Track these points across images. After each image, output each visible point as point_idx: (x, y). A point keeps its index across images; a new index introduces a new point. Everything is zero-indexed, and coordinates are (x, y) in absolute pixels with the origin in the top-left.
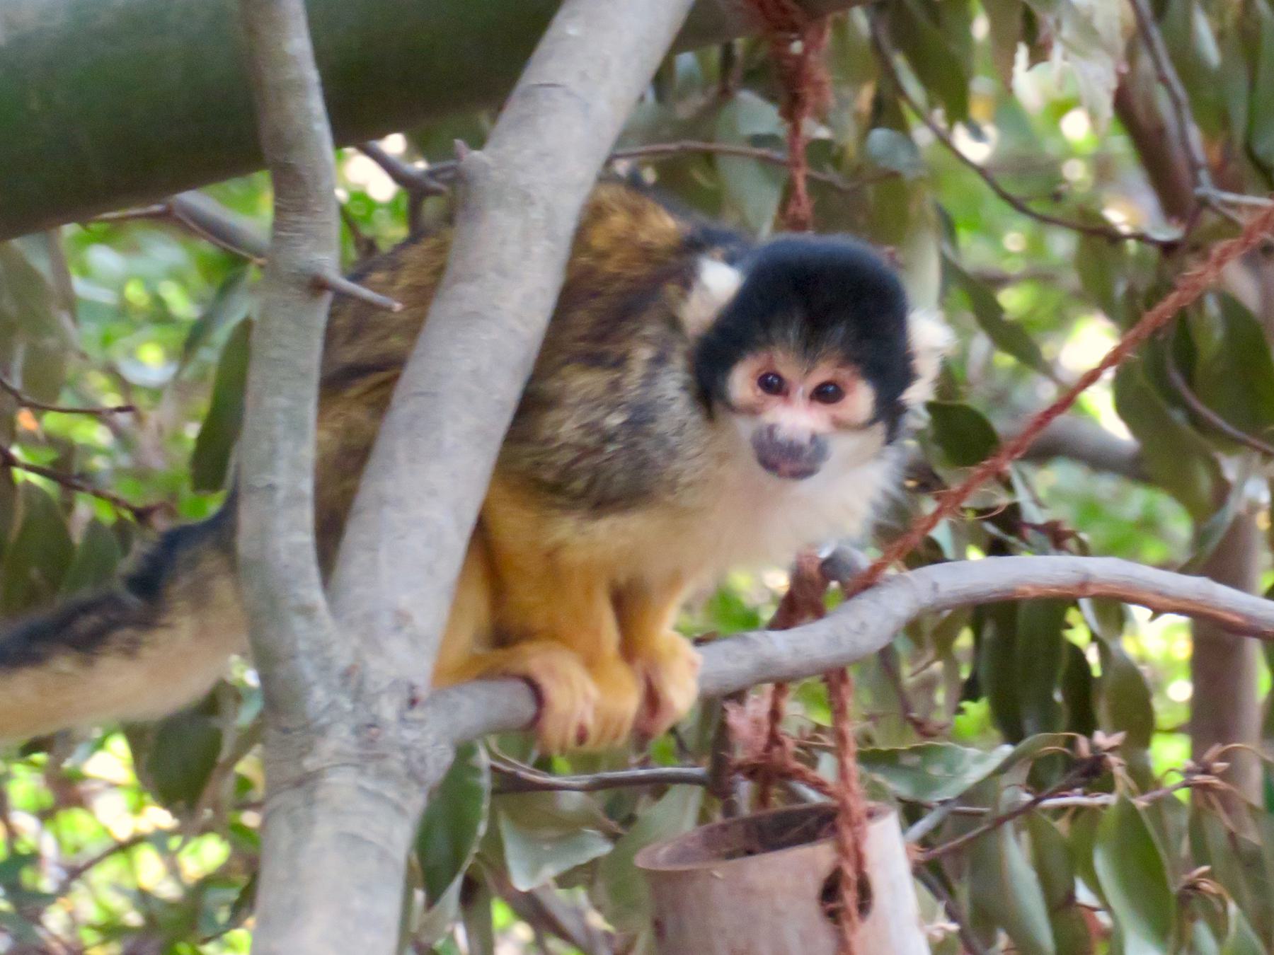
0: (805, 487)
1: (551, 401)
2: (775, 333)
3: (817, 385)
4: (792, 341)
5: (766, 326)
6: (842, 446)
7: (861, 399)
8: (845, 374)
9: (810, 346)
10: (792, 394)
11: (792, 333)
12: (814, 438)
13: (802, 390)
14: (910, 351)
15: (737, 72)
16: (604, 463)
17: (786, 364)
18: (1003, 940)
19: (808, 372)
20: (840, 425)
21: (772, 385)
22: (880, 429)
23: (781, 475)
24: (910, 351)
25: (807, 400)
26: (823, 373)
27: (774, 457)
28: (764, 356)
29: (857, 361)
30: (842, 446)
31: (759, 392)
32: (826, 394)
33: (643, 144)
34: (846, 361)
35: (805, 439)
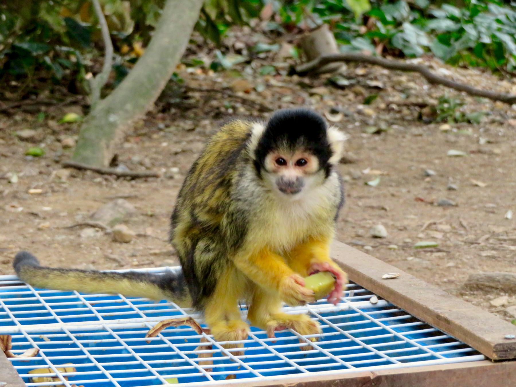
0: (297, 197)
1: (182, 293)
2: (279, 143)
3: (297, 160)
4: (285, 145)
5: (275, 142)
6: (309, 181)
7: (314, 163)
8: (306, 155)
9: (292, 145)
10: (288, 164)
11: (284, 142)
12: (298, 179)
13: (291, 162)
14: (282, 117)
15: (154, 161)
16: (230, 331)
17: (284, 154)
18: (157, 1)
19: (293, 155)
20: (306, 173)
21: (281, 162)
22: (322, 173)
23: (288, 194)
24: (282, 117)
25: (294, 165)
26: (298, 155)
27: (284, 188)
28: (276, 152)
29: (310, 149)
30: (309, 181)
31: (276, 165)
32: (300, 163)
33: (199, 209)
34: (306, 150)
35: (294, 180)
